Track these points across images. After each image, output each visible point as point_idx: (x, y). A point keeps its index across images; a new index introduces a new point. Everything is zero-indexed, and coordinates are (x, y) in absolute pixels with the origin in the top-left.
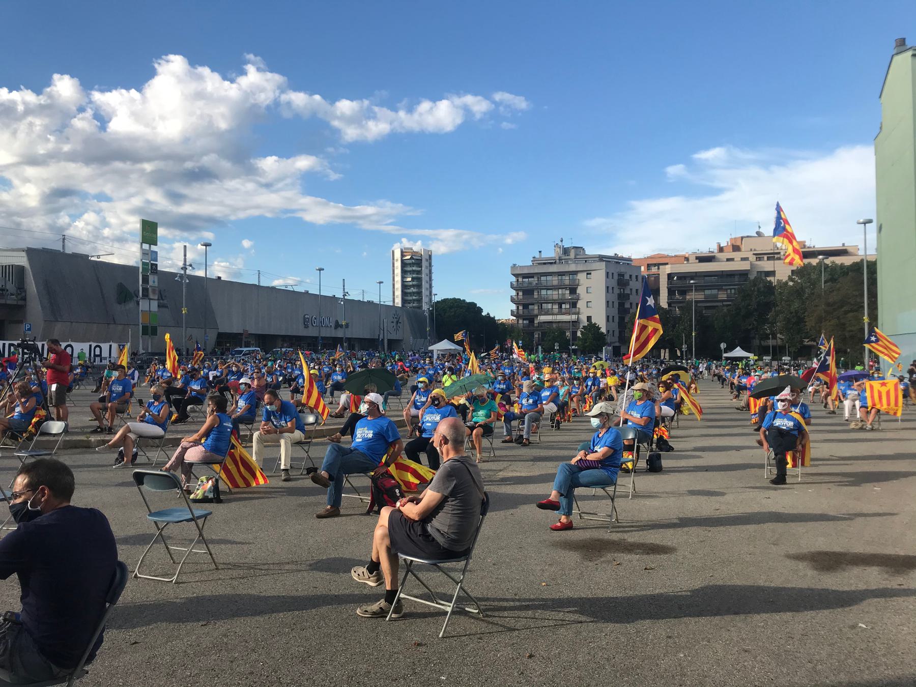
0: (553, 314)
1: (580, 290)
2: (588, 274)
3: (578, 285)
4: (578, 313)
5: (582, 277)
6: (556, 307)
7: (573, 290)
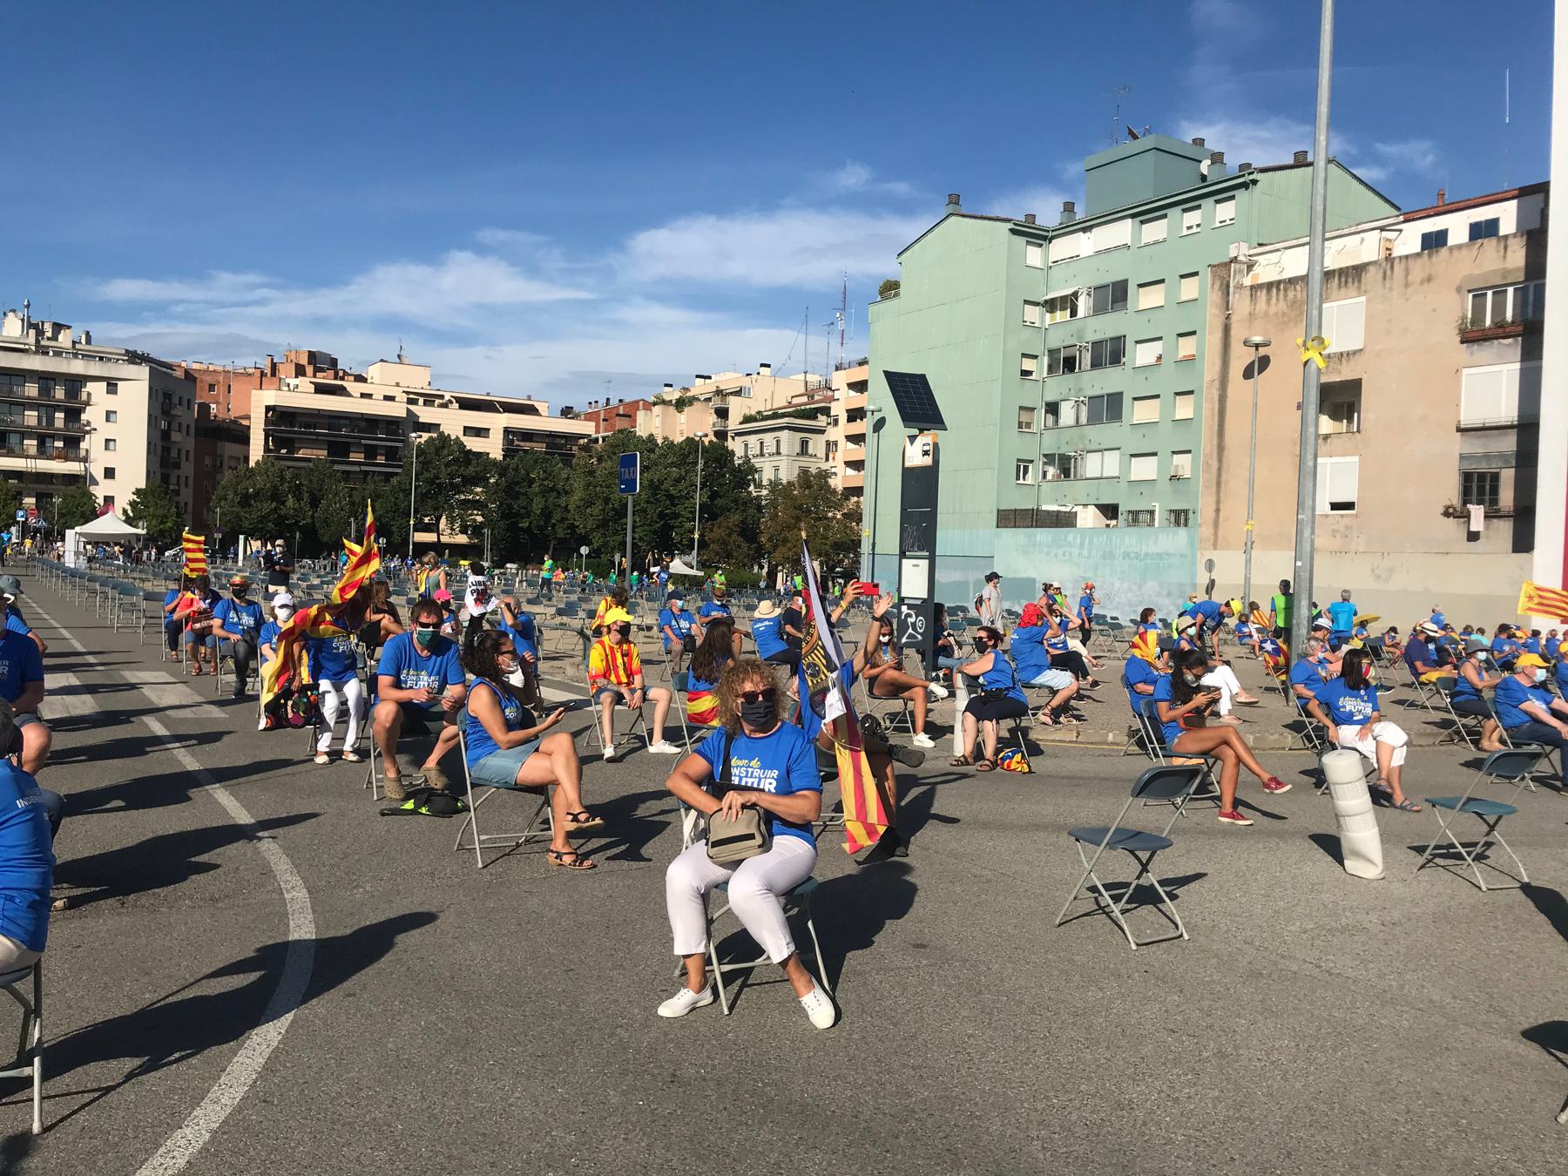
0: (27, 457)
1: (90, 415)
2: (108, 384)
3: (88, 403)
4: (85, 460)
5: (96, 390)
6: (31, 444)
7: (74, 414)
